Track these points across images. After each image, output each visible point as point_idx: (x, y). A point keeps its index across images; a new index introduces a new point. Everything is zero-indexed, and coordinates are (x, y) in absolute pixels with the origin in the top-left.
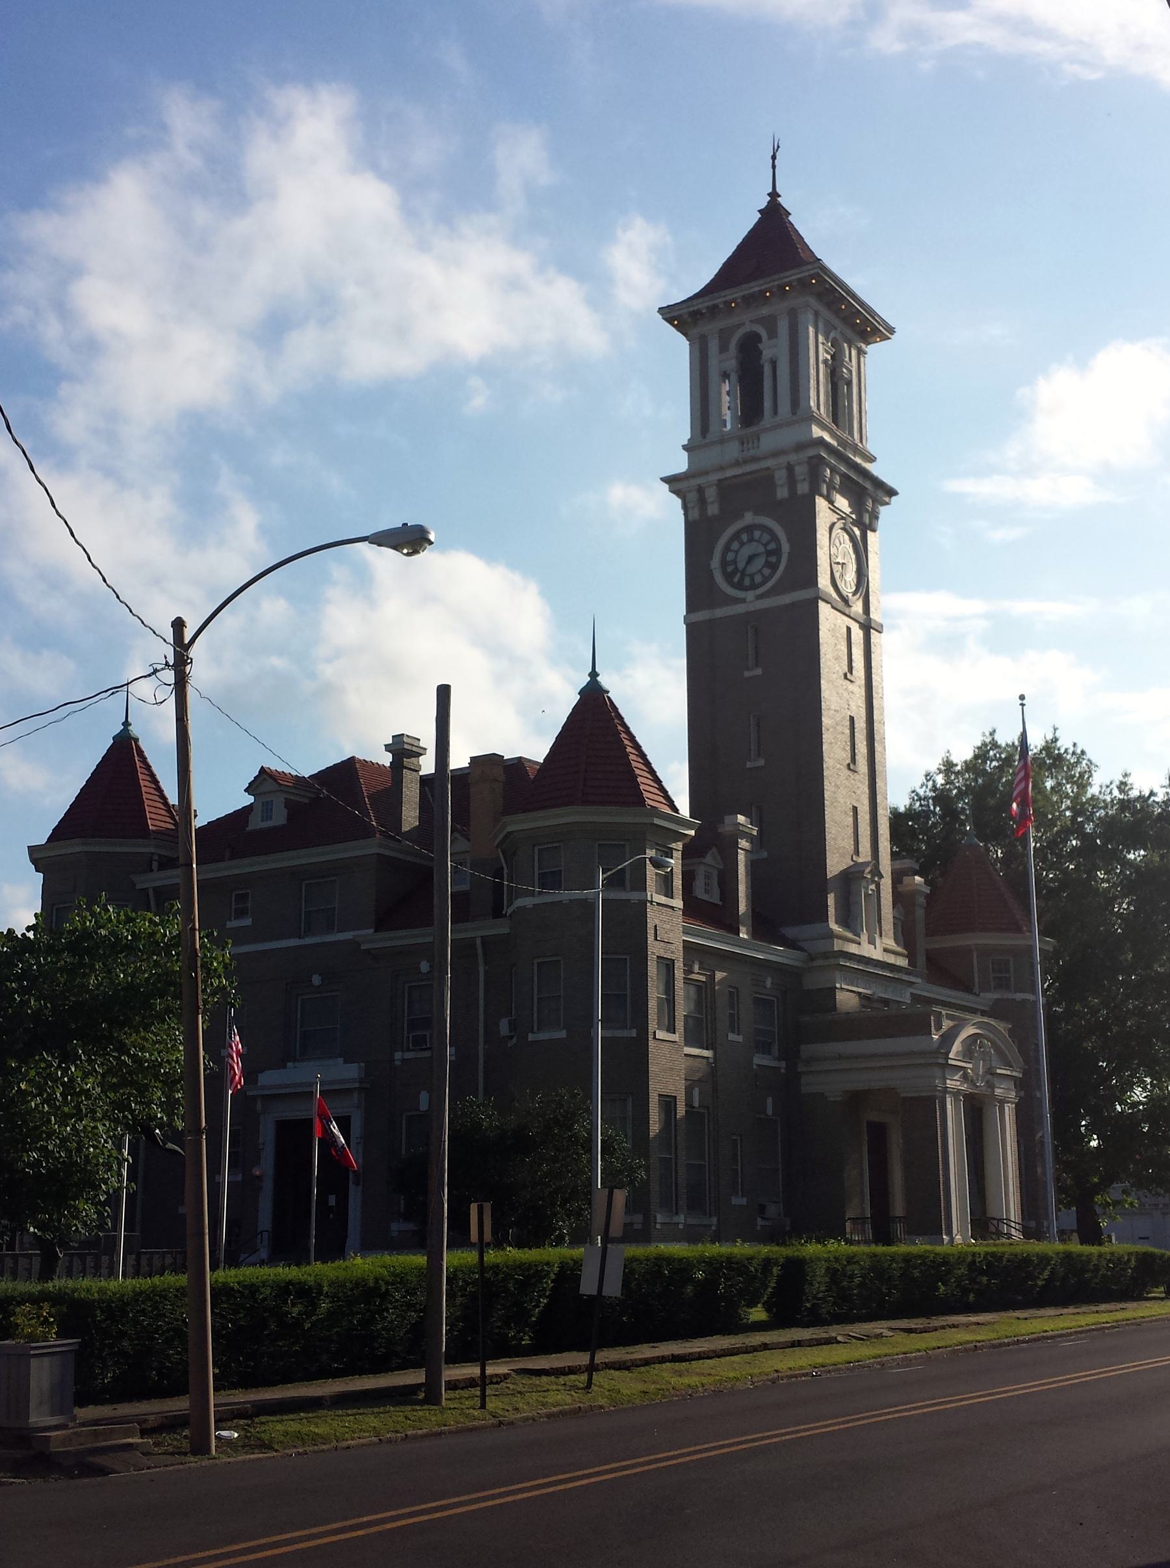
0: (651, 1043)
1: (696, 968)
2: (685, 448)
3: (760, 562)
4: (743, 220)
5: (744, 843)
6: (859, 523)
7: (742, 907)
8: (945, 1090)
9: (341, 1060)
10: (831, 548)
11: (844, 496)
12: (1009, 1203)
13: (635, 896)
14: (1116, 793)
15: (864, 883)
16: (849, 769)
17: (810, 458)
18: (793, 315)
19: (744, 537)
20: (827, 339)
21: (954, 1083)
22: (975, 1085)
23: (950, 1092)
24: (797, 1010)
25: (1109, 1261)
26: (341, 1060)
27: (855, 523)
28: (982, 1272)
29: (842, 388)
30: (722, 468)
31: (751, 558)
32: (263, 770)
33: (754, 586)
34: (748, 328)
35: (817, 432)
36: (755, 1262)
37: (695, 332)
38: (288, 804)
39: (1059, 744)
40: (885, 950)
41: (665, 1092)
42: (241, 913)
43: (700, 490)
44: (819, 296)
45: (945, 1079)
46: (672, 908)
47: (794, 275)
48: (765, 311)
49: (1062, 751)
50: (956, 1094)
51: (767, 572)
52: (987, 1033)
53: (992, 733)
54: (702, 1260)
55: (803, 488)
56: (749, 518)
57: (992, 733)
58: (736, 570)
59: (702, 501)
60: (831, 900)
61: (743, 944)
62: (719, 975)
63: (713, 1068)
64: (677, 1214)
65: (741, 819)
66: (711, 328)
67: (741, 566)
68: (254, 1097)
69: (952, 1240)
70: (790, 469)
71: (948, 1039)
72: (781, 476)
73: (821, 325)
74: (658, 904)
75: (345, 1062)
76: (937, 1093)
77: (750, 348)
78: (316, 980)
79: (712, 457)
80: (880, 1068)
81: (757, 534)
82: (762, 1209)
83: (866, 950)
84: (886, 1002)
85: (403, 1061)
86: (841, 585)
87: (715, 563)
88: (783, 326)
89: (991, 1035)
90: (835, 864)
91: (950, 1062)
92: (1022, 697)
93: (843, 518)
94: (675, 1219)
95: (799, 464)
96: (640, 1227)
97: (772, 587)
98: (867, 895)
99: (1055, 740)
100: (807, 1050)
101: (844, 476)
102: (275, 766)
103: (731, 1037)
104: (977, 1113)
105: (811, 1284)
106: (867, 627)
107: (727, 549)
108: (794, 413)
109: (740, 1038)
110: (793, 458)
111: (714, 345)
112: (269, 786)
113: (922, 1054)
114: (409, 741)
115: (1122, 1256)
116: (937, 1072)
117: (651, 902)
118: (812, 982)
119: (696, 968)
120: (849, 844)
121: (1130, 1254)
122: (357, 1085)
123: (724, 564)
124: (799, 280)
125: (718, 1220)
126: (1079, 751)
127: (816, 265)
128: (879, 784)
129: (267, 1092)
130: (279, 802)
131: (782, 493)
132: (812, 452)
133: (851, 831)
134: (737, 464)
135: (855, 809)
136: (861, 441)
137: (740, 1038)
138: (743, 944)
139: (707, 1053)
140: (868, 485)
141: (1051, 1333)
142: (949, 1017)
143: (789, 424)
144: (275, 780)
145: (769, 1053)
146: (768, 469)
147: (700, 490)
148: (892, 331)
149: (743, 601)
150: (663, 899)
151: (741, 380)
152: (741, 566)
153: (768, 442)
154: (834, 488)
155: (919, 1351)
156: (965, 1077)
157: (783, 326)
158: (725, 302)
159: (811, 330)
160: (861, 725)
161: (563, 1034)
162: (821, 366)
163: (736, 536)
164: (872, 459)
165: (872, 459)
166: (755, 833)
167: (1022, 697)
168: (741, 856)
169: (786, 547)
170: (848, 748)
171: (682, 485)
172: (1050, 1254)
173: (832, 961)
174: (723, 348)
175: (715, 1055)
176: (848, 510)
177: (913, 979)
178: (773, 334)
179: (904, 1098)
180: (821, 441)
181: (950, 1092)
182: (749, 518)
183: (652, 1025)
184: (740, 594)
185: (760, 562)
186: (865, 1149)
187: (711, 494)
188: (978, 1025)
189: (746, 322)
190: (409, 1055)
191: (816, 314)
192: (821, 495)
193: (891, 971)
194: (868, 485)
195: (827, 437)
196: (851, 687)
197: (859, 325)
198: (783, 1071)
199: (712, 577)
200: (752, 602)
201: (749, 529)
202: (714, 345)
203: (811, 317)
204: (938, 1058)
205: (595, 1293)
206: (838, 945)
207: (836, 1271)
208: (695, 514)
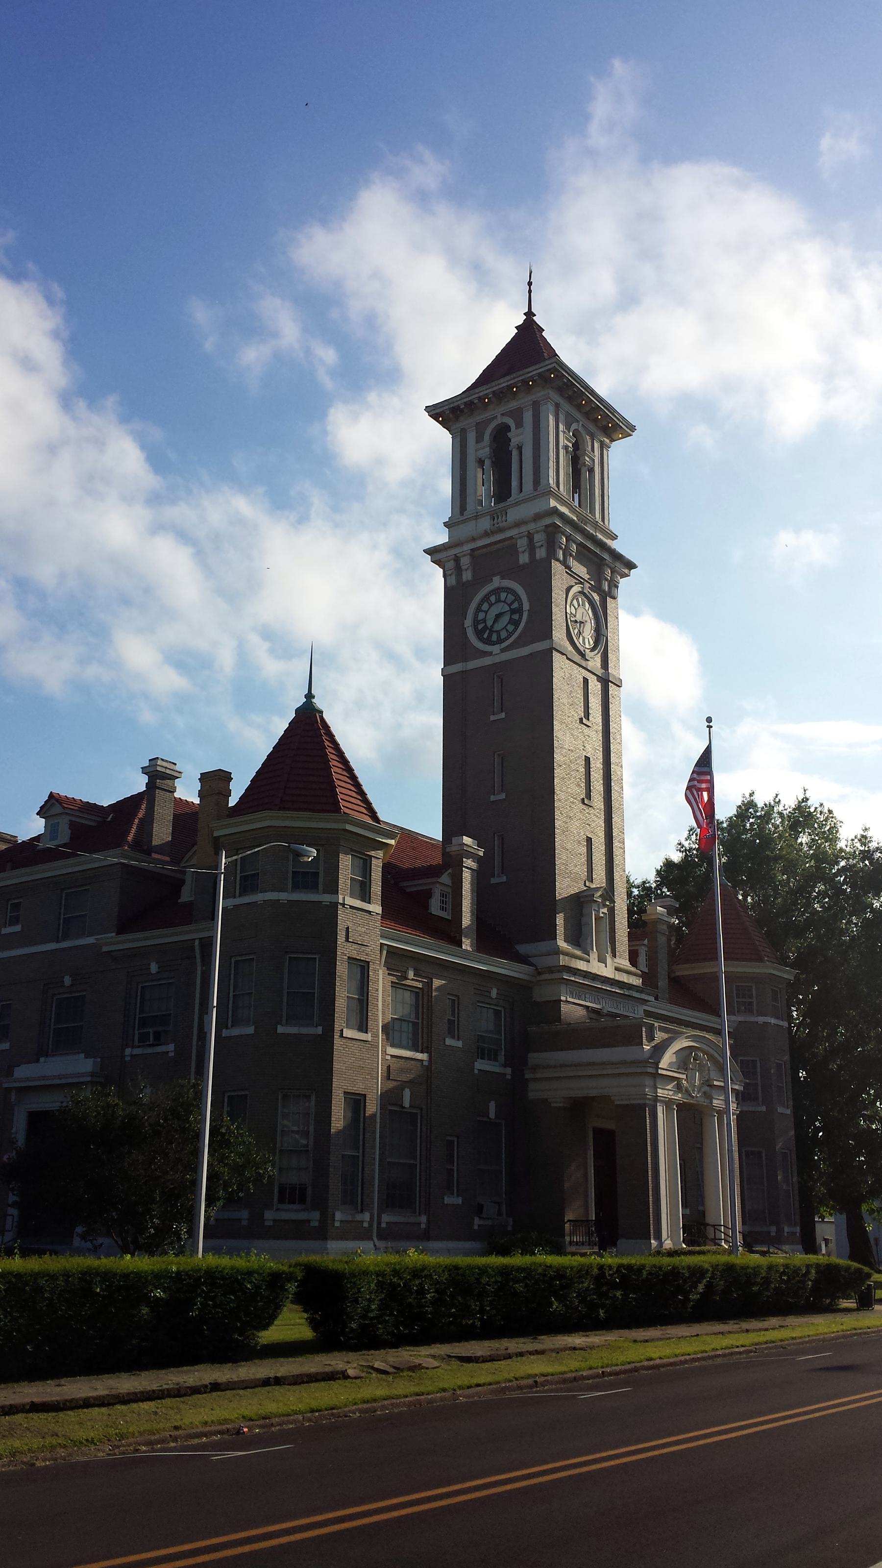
0: (337, 1041)
1: (411, 974)
2: (446, 524)
3: (506, 619)
5: (469, 862)
6: (597, 588)
7: (467, 920)
8: (656, 1099)
9: (82, 1055)
10: (567, 604)
11: (581, 562)
12: (725, 1205)
13: (326, 898)
14: (858, 845)
15: (595, 907)
16: (583, 802)
17: (546, 526)
18: (536, 406)
19: (493, 599)
20: (568, 427)
21: (665, 1092)
22: (690, 1095)
23: (661, 1101)
24: (528, 1021)
25: (784, 1273)
26: (82, 1055)
27: (592, 588)
28: (614, 1286)
29: (582, 474)
30: (474, 539)
31: (498, 617)
32: (51, 795)
33: (500, 641)
34: (499, 420)
35: (553, 503)
36: (255, 1278)
37: (458, 426)
38: (72, 825)
39: (809, 803)
40: (617, 969)
41: (351, 1089)
42: (15, 921)
43: (457, 559)
44: (560, 390)
45: (656, 1088)
46: (369, 912)
47: (534, 371)
48: (513, 405)
49: (812, 810)
50: (668, 1103)
51: (511, 628)
52: (704, 1047)
54: (159, 1277)
55: (541, 553)
56: (497, 582)
57: (751, 795)
58: (486, 627)
59: (458, 569)
60: (560, 920)
61: (465, 955)
62: (437, 983)
63: (428, 1069)
64: (362, 1211)
65: (467, 840)
66: (468, 422)
67: (489, 623)
68: (9, 1089)
69: (661, 1244)
70: (530, 537)
71: (659, 1050)
72: (522, 543)
73: (562, 417)
74: (351, 907)
75: (86, 1057)
76: (647, 1102)
77: (501, 436)
78: (67, 981)
79: (468, 529)
80: (619, 1075)
81: (503, 596)
82: (480, 1209)
83: (595, 967)
84: (614, 1016)
85: (132, 1056)
86: (579, 642)
87: (468, 622)
88: (528, 417)
89: (704, 1047)
90: (566, 886)
91: (660, 1071)
92: (709, 720)
93: (581, 583)
94: (359, 1217)
95: (537, 532)
96: (316, 1224)
97: (515, 641)
98: (598, 918)
99: (806, 800)
100: (535, 1058)
101: (580, 545)
102: (66, 791)
103: (449, 1041)
104: (692, 1120)
105: (356, 1301)
106: (606, 682)
107: (478, 609)
108: (535, 489)
109: (460, 1044)
110: (531, 527)
111: (471, 436)
112: (57, 809)
113: (633, 1063)
114: (164, 764)
115: (799, 1269)
116: (648, 1081)
117: (343, 905)
118: (542, 994)
119: (411, 974)
120: (583, 871)
121: (808, 1266)
122: (89, 1079)
123: (476, 622)
124: (540, 375)
126: (826, 810)
127: (553, 360)
128: (615, 819)
129: (22, 1084)
130: (64, 824)
131: (524, 558)
132: (547, 521)
133: (584, 859)
134: (486, 534)
136: (603, 520)
137: (460, 1044)
138: (465, 955)
139: (423, 1056)
140: (606, 556)
141: (658, 1361)
142: (662, 1029)
143: (534, 498)
144: (60, 804)
145: (496, 1060)
146: (511, 538)
147: (457, 559)
148: (633, 428)
149: (489, 654)
150: (358, 903)
151: (494, 464)
152: (489, 623)
153: (513, 515)
154: (571, 555)
155: (444, 1390)
156: (679, 1088)
157: (528, 417)
158: (479, 398)
159: (551, 418)
160: (597, 765)
161: (251, 1030)
162: (562, 452)
163: (486, 598)
164: (614, 537)
165: (614, 537)
166: (481, 854)
167: (709, 720)
168: (467, 875)
169: (526, 606)
170: (583, 785)
172: (706, 1266)
173: (556, 976)
174: (479, 439)
175: (430, 1057)
176: (586, 577)
178: (519, 424)
179: (617, 1105)
180: (555, 511)
181: (661, 1101)
182: (497, 582)
183: (339, 1022)
184: (487, 648)
185: (506, 619)
186: (591, 1153)
187: (465, 561)
188: (694, 1038)
189: (498, 415)
190: (137, 1051)
191: (557, 406)
192: (558, 560)
193: (621, 988)
194: (606, 556)
195: (563, 509)
196: (586, 731)
197: (602, 422)
198: (509, 1077)
199: (466, 637)
200: (497, 655)
201: (497, 591)
202: (471, 436)
203: (551, 408)
205: (834, 1226)
206: (563, 960)
207: (394, 1286)
208: (453, 581)
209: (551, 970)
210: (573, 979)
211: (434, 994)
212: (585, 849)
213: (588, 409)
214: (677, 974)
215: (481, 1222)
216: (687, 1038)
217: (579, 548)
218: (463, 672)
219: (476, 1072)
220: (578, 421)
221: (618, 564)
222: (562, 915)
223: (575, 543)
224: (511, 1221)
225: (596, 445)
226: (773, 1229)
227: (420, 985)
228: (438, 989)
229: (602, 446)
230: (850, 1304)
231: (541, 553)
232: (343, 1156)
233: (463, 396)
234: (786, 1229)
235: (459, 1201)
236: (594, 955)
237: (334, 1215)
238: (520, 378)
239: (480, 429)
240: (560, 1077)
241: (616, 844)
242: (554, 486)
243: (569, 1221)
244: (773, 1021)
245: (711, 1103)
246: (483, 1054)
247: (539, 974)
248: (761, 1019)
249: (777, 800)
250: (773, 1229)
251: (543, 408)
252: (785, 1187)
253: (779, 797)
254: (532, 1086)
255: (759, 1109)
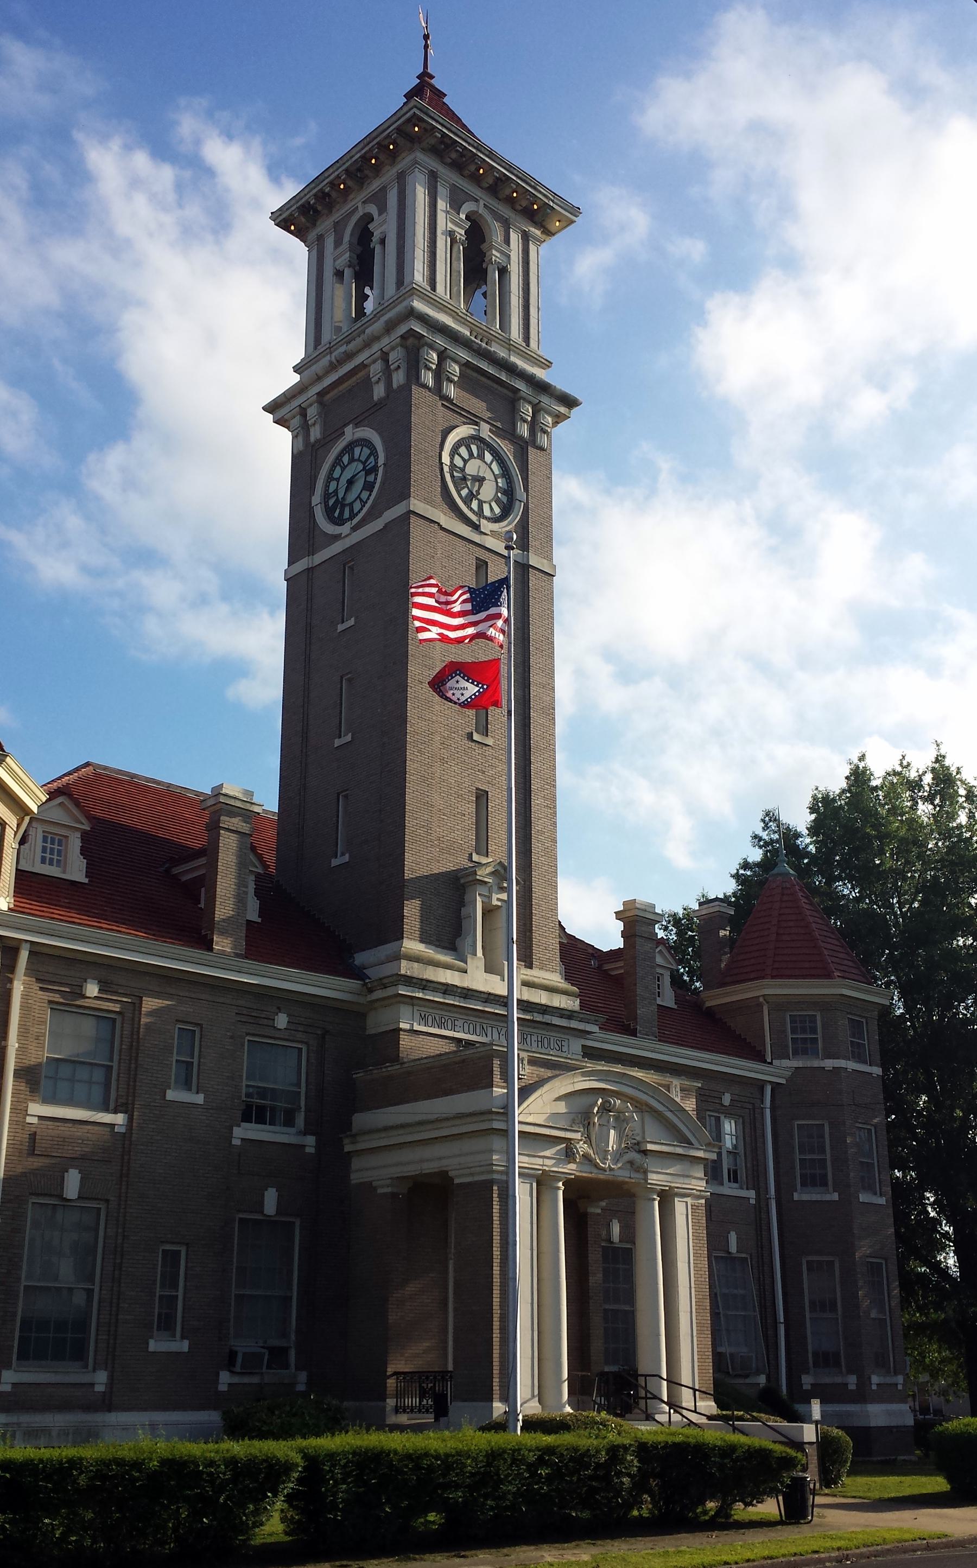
1: (92, 989)
3: (359, 485)
4: (382, 104)
6: (509, 433)
17: (402, 337)
18: (401, 178)
19: (346, 459)
20: (456, 205)
22: (596, 1166)
24: (353, 1066)
31: (350, 482)
43: (303, 412)
48: (375, 185)
50: (542, 1181)
51: (365, 495)
53: (862, 758)
55: (399, 378)
57: (862, 758)
62: (150, 1004)
64: (94, 1370)
66: (325, 225)
72: (376, 369)
76: (495, 1176)
77: (364, 236)
81: (357, 450)
87: (316, 499)
90: (422, 858)
95: (393, 349)
98: (489, 912)
101: (466, 365)
107: (330, 478)
109: (200, 1099)
110: (385, 341)
111: (329, 242)
118: (377, 1023)
119: (92, 989)
123: (326, 496)
125: (111, 1378)
131: (379, 392)
132: (402, 329)
135: (482, 797)
136: (527, 339)
137: (200, 1099)
140: (520, 385)
149: (337, 537)
152: (341, 495)
163: (338, 461)
165: (547, 365)
171: (282, 412)
173: (390, 991)
174: (338, 243)
175: (130, 1119)
177: (589, 1027)
178: (382, 209)
182: (350, 433)
185: (359, 485)
187: (312, 412)
194: (520, 385)
198: (753, 1201)
200: (348, 536)
202: (329, 242)
204: (496, 1122)
209: (383, 983)
210: (420, 995)
211: (144, 1020)
212: (472, 808)
213: (491, 181)
214: (708, 1004)
215: (236, 1380)
216: (583, 1074)
217: (463, 368)
218: (308, 569)
219: (236, 1142)
220: (477, 201)
221: (545, 400)
222: (417, 902)
223: (456, 362)
224: (303, 1377)
225: (514, 237)
226: (852, 1381)
227: (117, 1008)
228: (150, 1014)
229: (526, 237)
230: (770, 1508)
231: (399, 378)
232: (605, 1310)
233: (313, 185)
234: (875, 1379)
235: (185, 1346)
236: (476, 963)
237: (870, 1378)
238: (375, 142)
239: (338, 228)
240: (392, 1149)
241: (536, 801)
242: (520, 341)
243: (395, 1373)
244: (851, 1065)
245: (646, 1179)
246: (254, 1113)
247: (371, 991)
248: (829, 1064)
249: (905, 763)
250: (852, 1381)
251: (409, 179)
252: (873, 1314)
253: (907, 759)
254: (356, 1163)
255: (827, 1197)
